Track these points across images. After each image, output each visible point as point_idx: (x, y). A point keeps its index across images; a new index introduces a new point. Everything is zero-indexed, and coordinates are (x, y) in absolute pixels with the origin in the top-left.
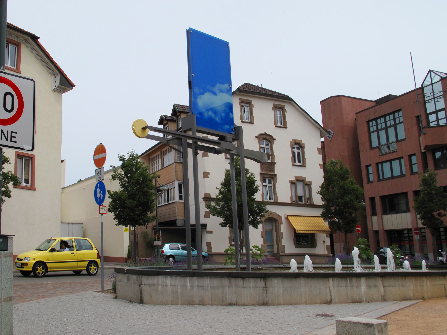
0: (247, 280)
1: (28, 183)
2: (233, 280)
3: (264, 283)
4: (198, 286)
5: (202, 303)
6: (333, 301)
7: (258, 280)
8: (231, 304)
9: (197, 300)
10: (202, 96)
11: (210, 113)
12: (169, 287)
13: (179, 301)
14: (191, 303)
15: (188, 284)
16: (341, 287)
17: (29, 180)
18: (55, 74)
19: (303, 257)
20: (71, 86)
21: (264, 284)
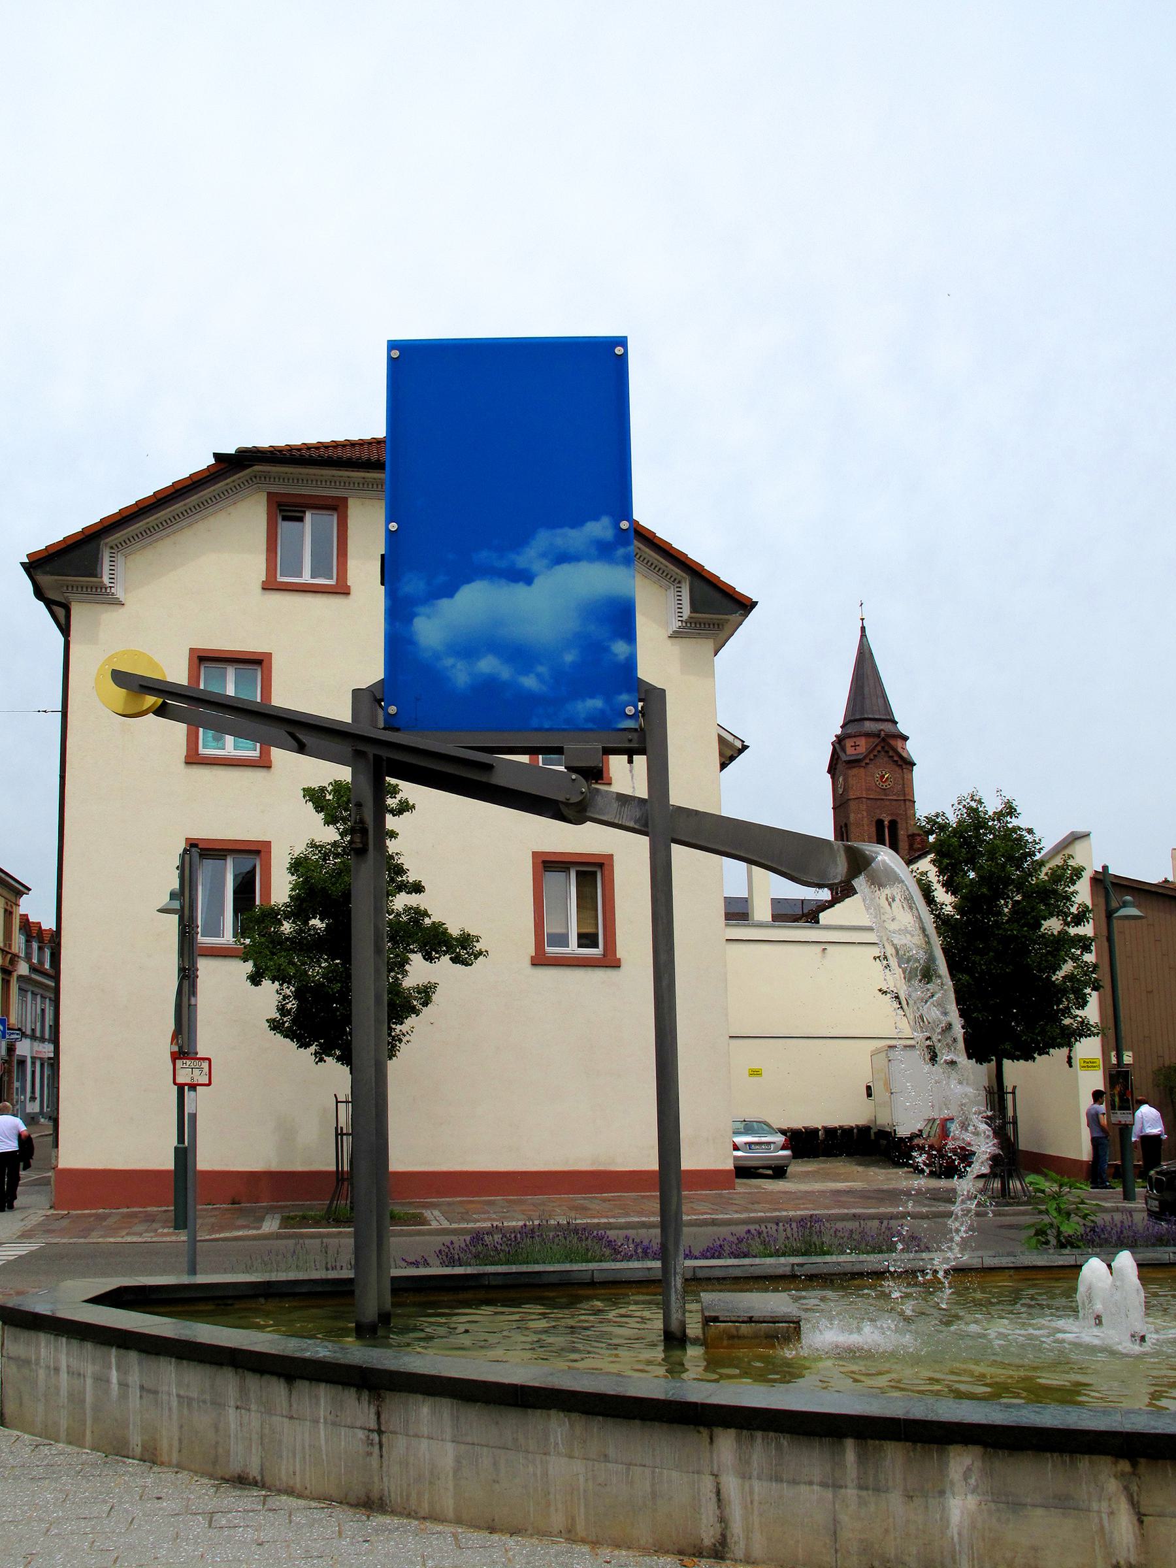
0: (302, 1386)
1: (595, 945)
2: (253, 1382)
3: (373, 1410)
4: (142, 1388)
5: (151, 1457)
6: (738, 1550)
7: (350, 1396)
8: (241, 1481)
9: (136, 1440)
10: (444, 603)
11: (488, 665)
12: (64, 1376)
13: (88, 1433)
14: (115, 1448)
15: (114, 1376)
16: (794, 1482)
17: (597, 935)
18: (677, 582)
19: (1075, 1271)
20: (745, 606)
21: (373, 1417)
